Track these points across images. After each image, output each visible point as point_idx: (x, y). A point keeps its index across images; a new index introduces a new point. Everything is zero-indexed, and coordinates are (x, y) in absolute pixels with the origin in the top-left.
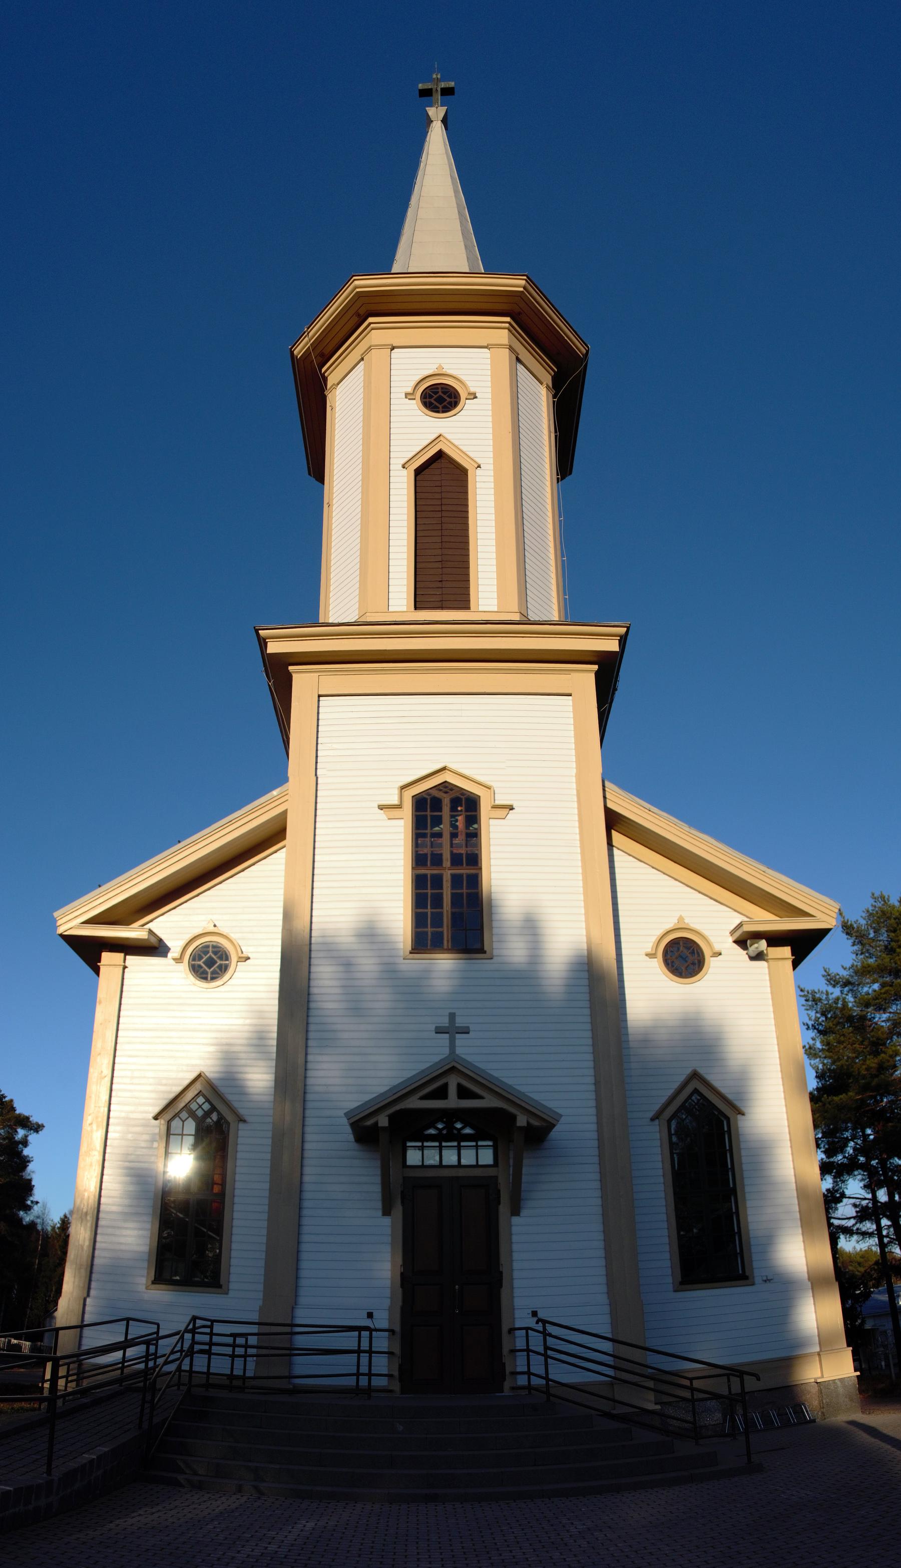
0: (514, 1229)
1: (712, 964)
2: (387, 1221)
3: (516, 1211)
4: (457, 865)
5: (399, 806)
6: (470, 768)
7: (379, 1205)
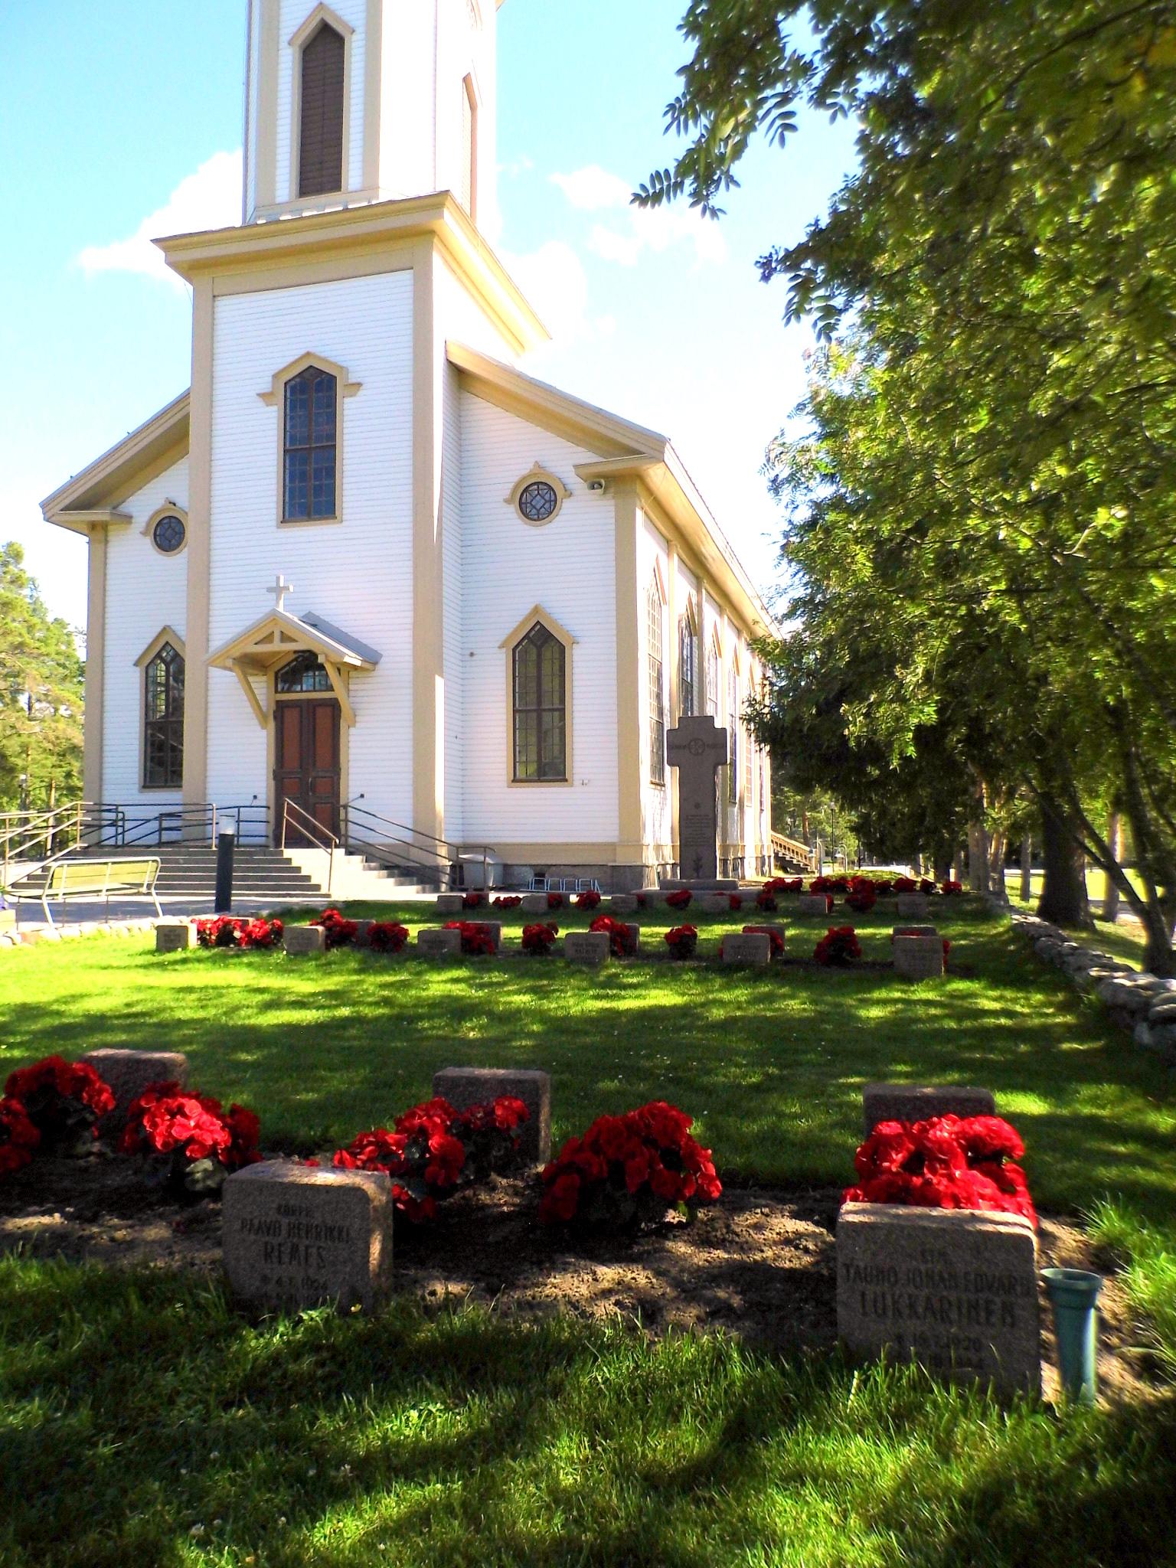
0: (351, 738)
1: (567, 509)
2: (264, 732)
3: (353, 723)
4: (320, 190)
5: (271, 394)
6: (332, 348)
7: (256, 722)
